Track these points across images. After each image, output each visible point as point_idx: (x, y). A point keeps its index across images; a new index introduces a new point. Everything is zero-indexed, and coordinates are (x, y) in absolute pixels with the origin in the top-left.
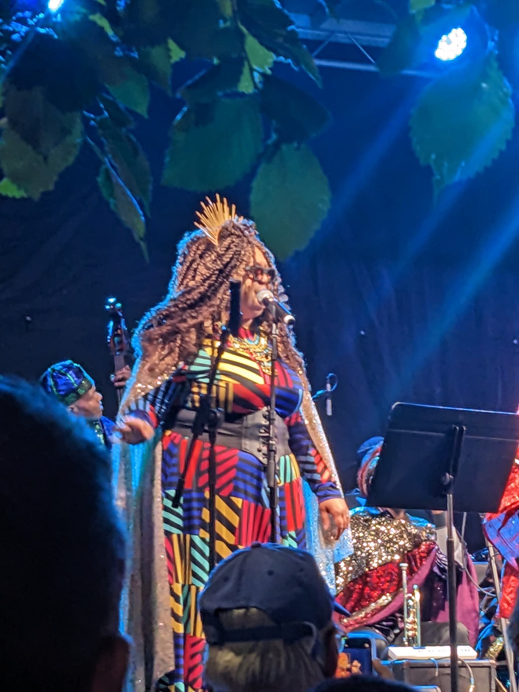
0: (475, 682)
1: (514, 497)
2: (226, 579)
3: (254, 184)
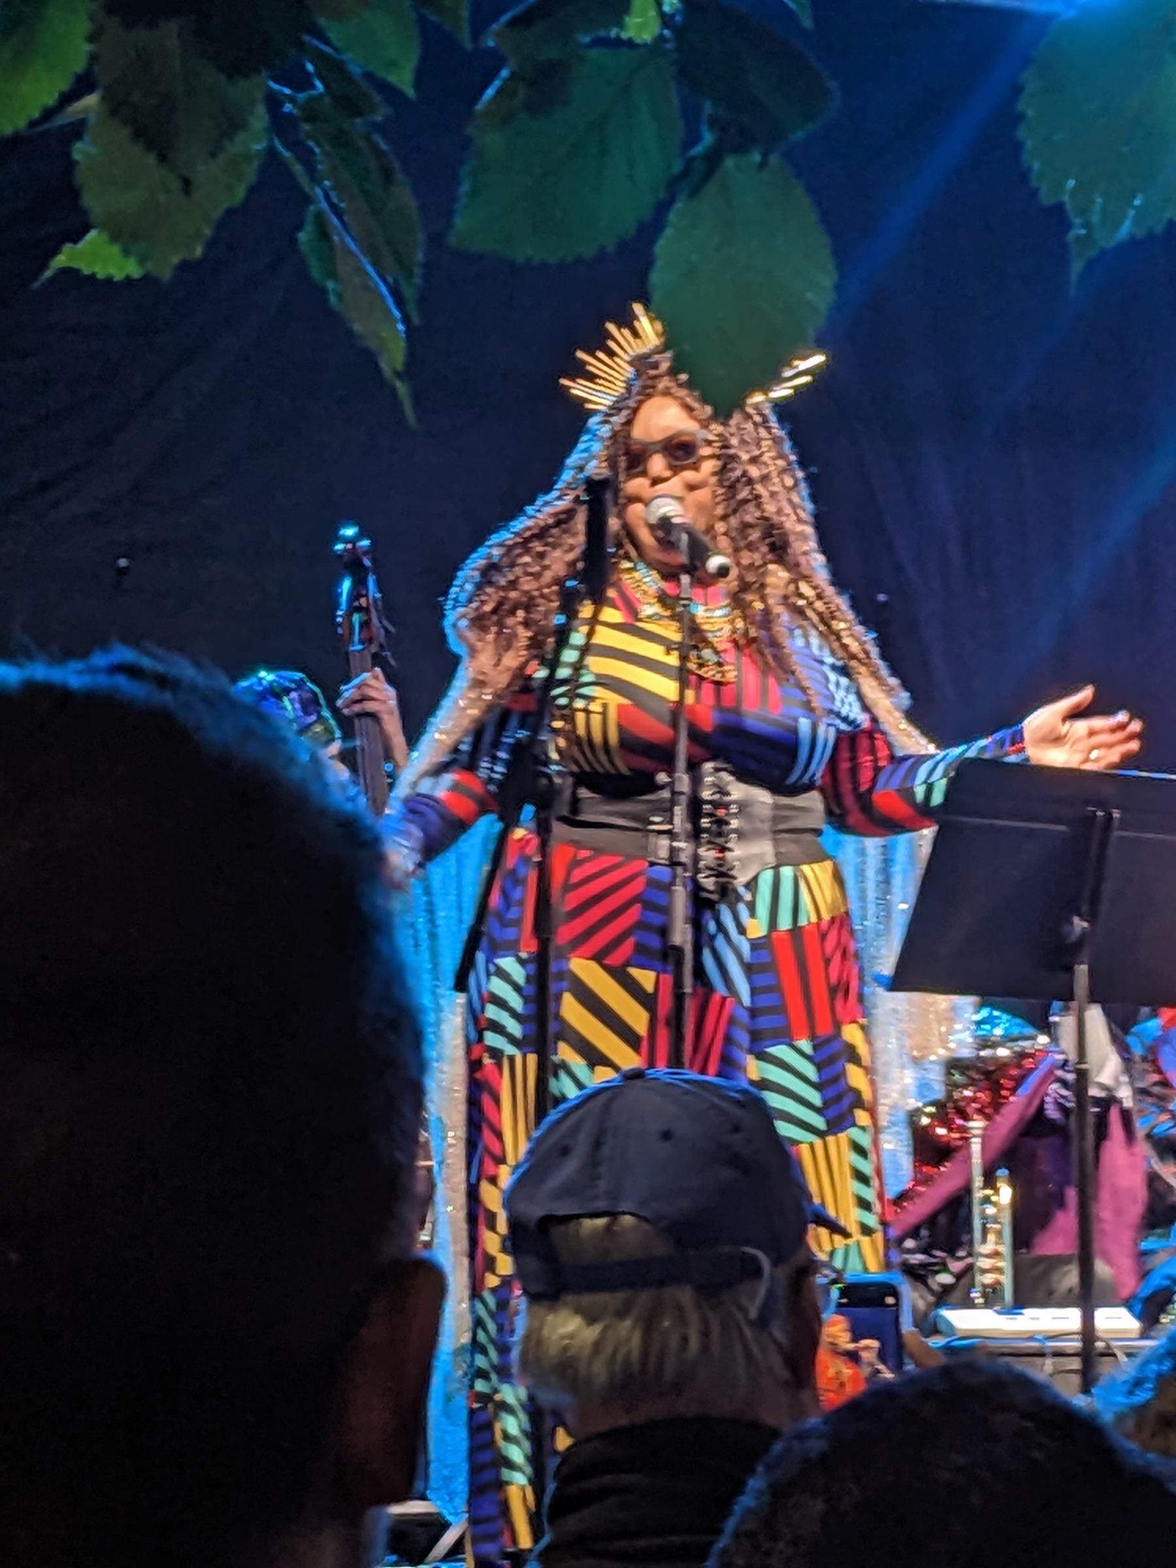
2: (565, 1151)
3: (661, 247)
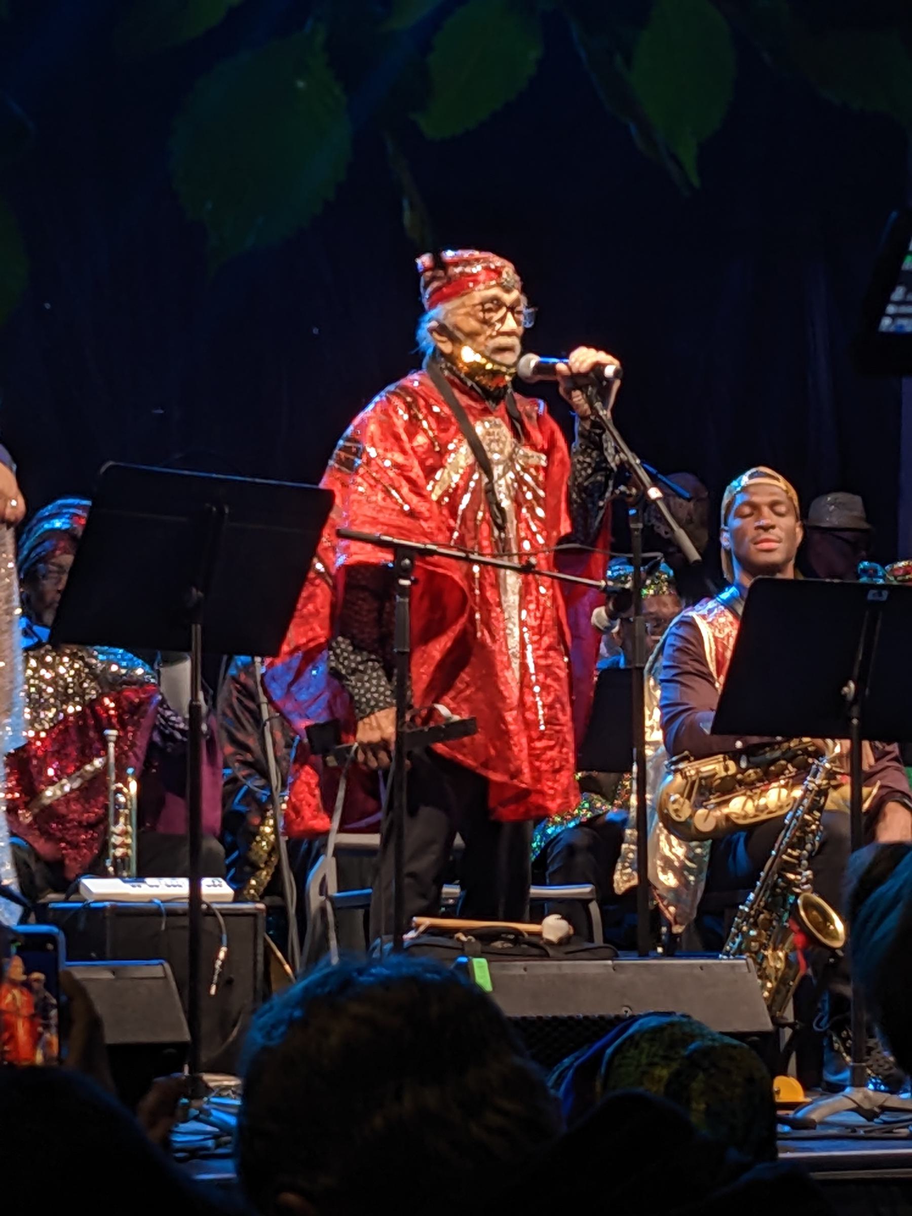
0: (228, 940)
1: (312, 629)
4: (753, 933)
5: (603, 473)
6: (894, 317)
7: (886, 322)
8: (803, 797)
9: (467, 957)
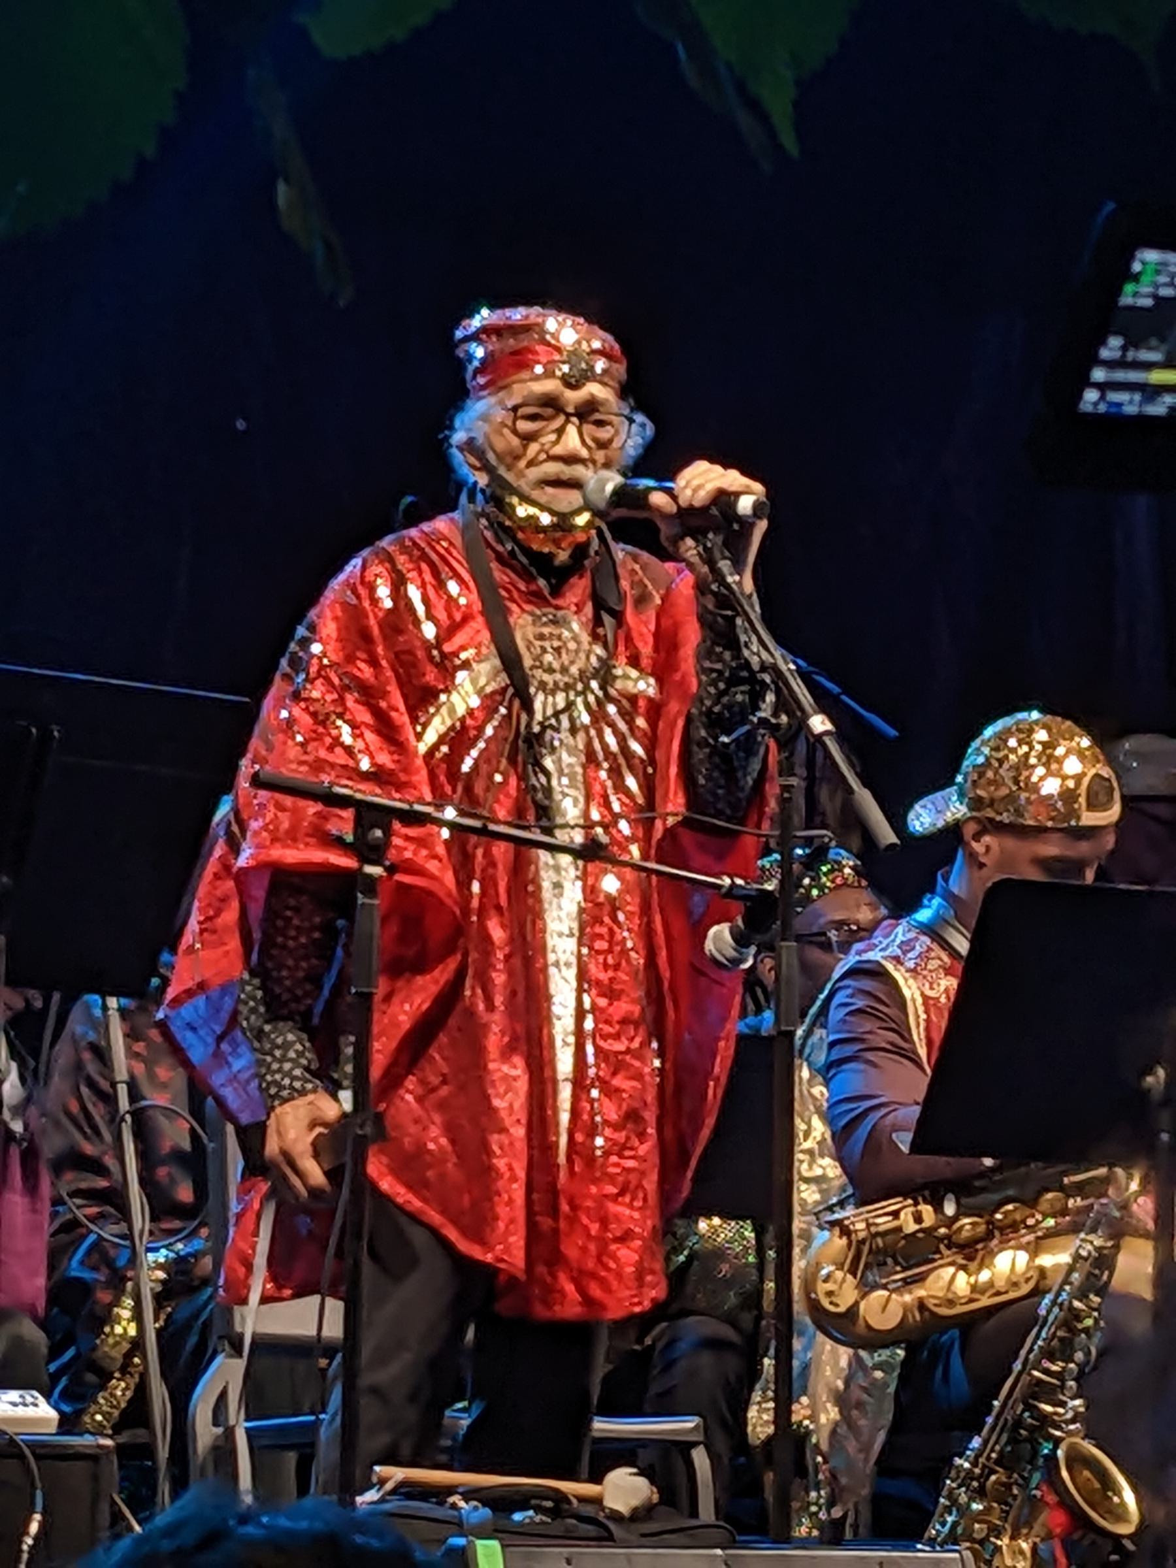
4: (976, 1506)
5: (745, 688)
6: (1103, 387)
7: (1091, 395)
8: (1071, 1269)
9: (466, 1536)
